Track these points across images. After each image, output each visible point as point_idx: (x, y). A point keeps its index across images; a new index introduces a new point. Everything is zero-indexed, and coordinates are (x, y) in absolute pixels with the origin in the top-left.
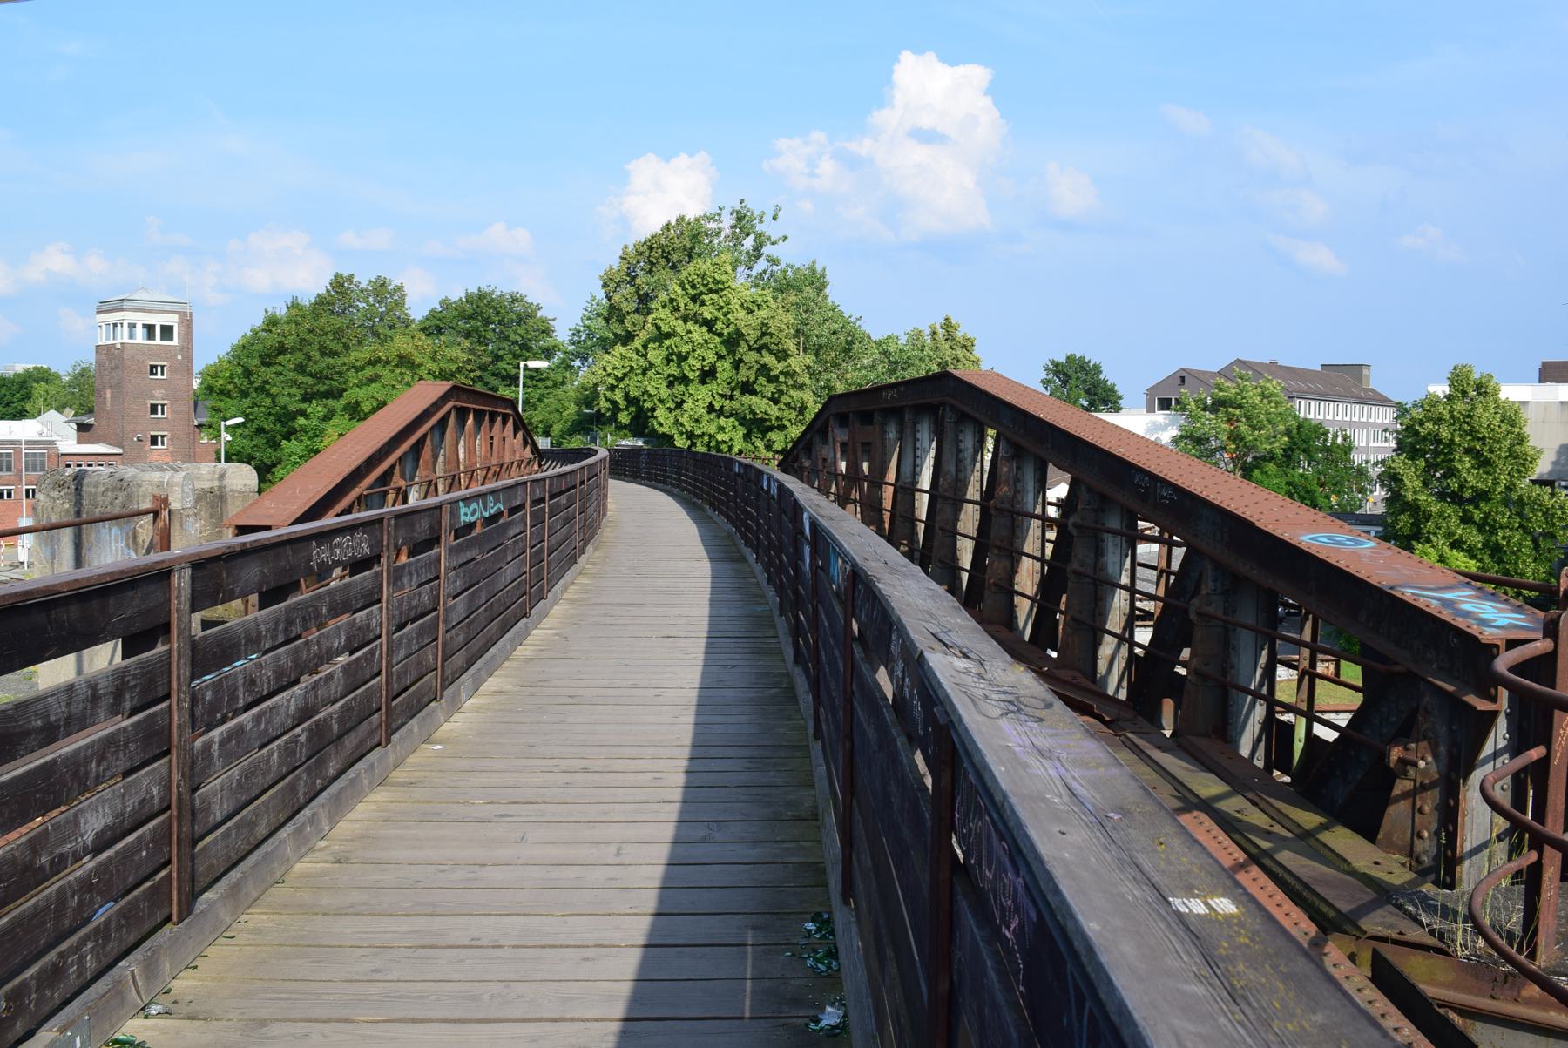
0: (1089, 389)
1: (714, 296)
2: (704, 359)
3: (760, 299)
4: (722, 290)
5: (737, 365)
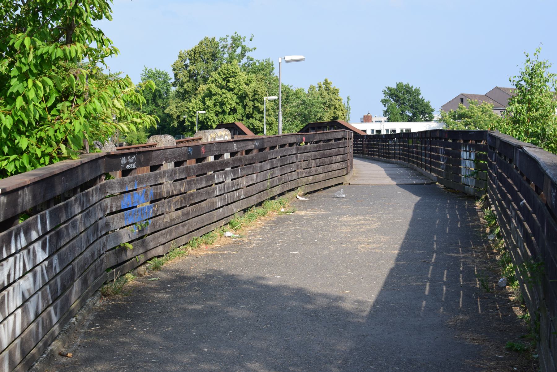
0: (412, 105)
1: (233, 78)
2: (231, 105)
3: (250, 79)
4: (236, 76)
5: (244, 107)
